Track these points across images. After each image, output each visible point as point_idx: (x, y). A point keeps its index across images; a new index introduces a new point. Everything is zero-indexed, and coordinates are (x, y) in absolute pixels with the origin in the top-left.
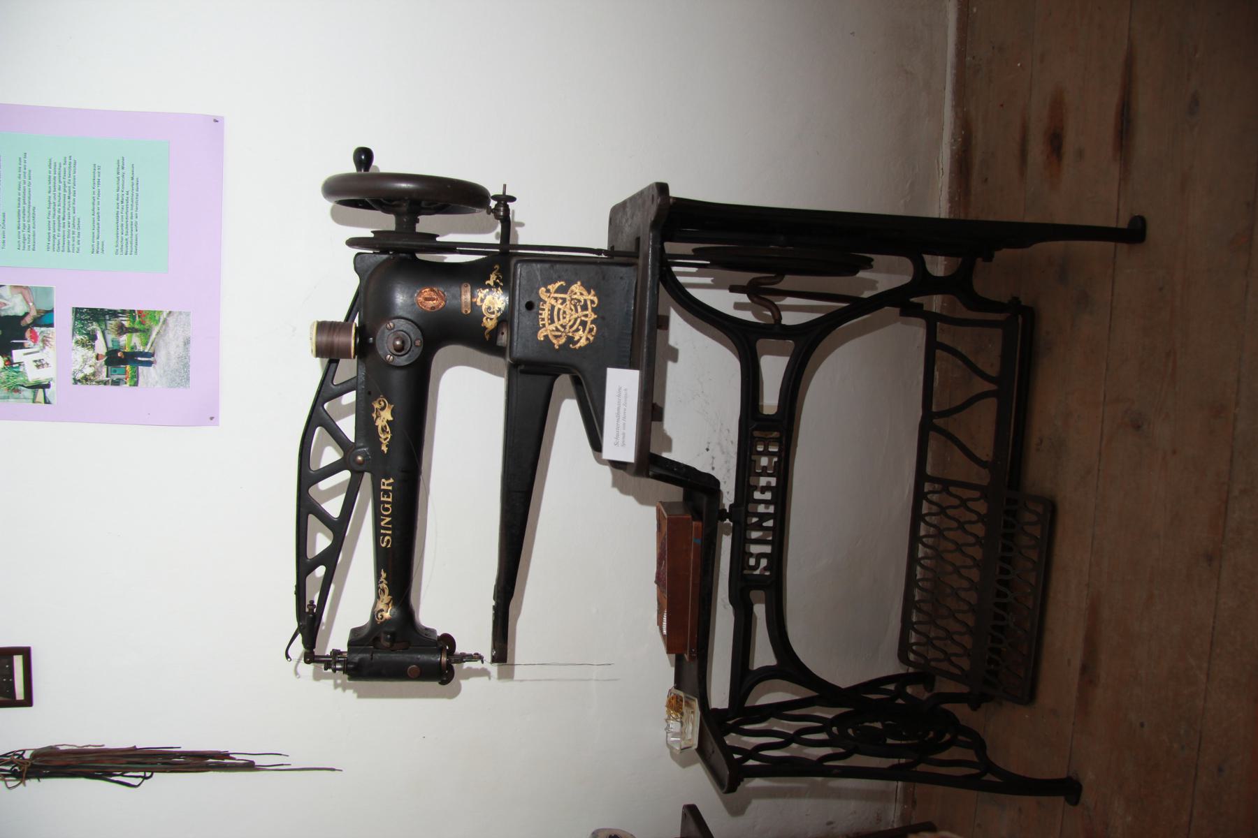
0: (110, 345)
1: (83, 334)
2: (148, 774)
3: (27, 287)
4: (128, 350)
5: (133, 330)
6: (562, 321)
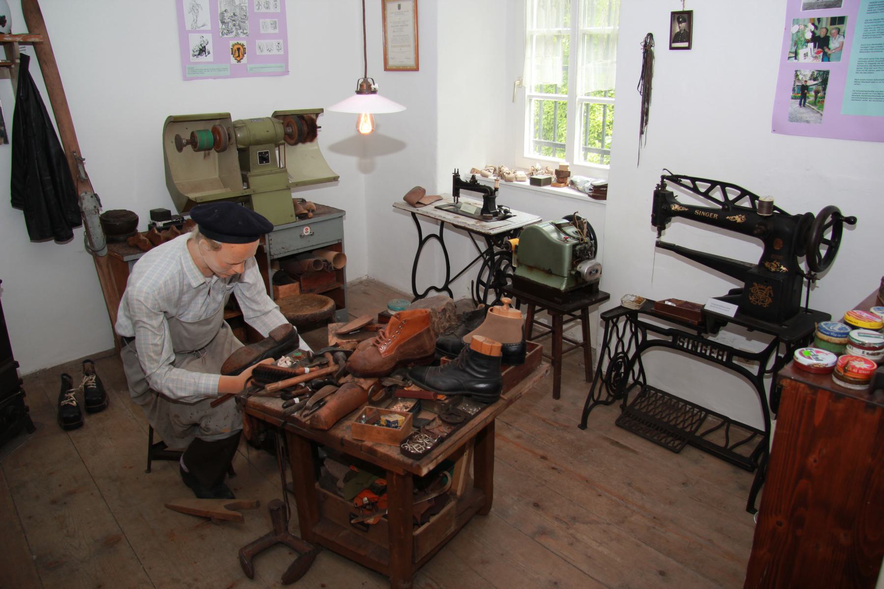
0: (811, 87)
1: (817, 75)
2: (642, 94)
3: (842, 49)
4: (808, 95)
5: (816, 97)
6: (759, 293)
